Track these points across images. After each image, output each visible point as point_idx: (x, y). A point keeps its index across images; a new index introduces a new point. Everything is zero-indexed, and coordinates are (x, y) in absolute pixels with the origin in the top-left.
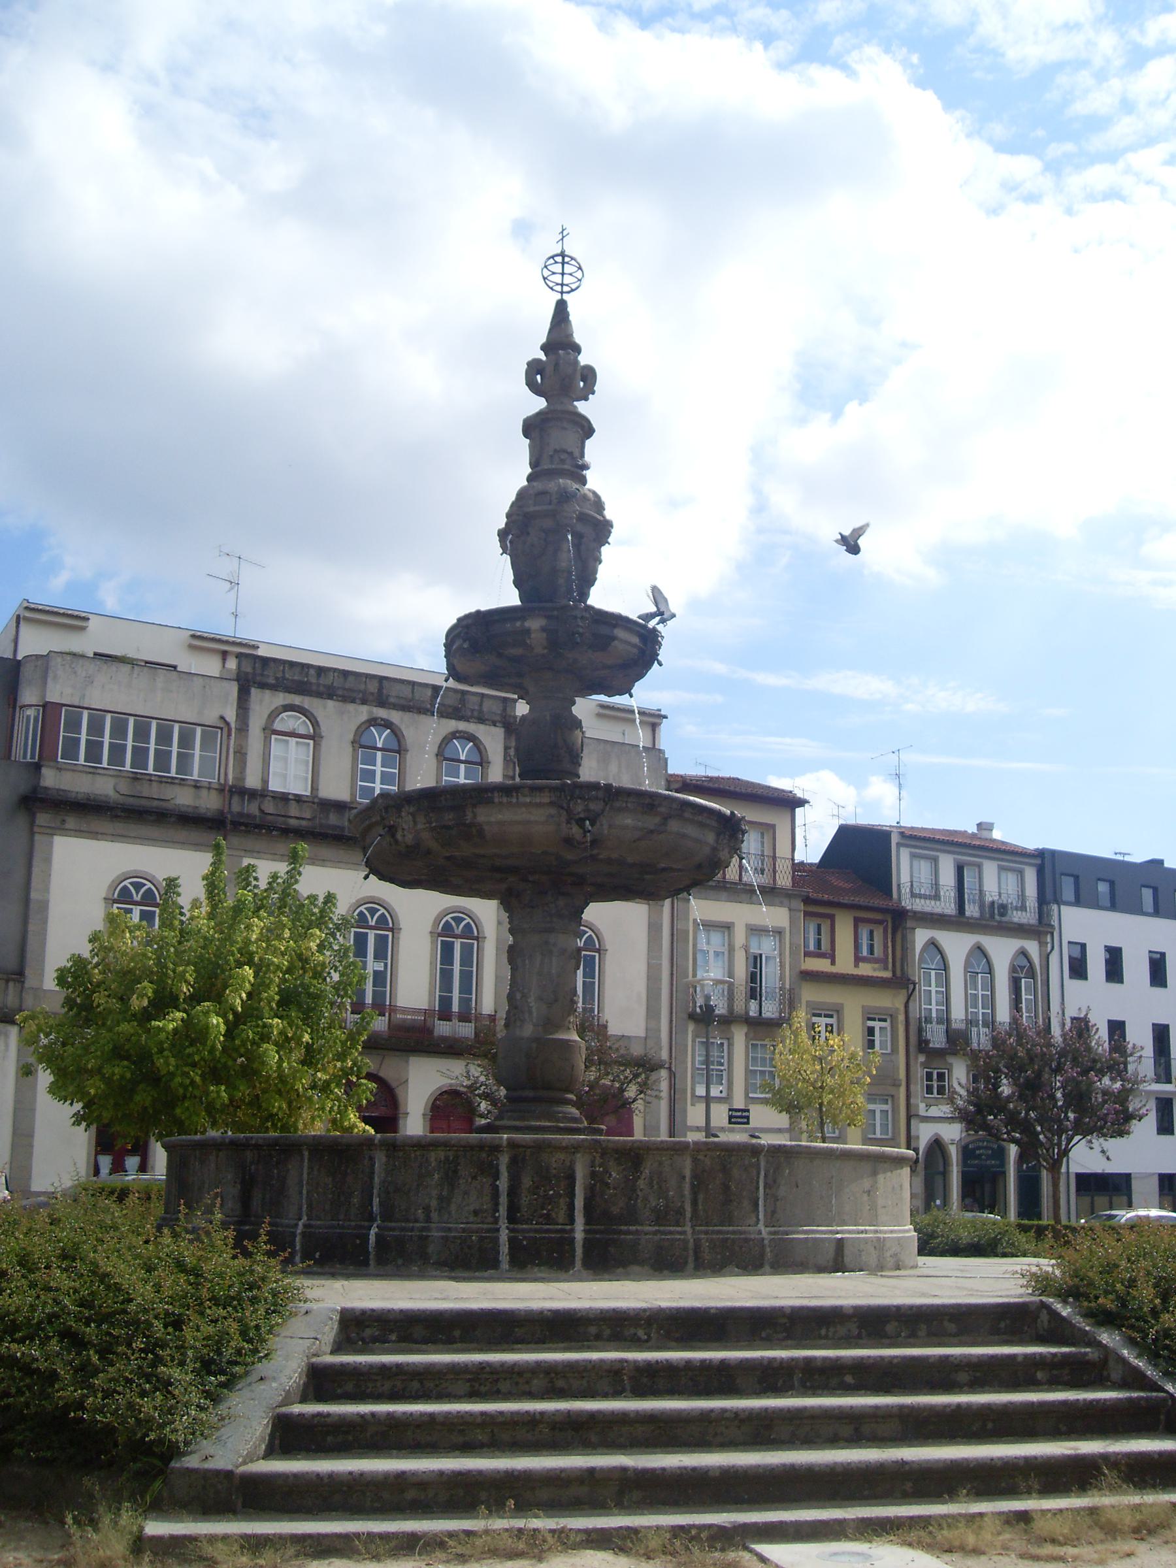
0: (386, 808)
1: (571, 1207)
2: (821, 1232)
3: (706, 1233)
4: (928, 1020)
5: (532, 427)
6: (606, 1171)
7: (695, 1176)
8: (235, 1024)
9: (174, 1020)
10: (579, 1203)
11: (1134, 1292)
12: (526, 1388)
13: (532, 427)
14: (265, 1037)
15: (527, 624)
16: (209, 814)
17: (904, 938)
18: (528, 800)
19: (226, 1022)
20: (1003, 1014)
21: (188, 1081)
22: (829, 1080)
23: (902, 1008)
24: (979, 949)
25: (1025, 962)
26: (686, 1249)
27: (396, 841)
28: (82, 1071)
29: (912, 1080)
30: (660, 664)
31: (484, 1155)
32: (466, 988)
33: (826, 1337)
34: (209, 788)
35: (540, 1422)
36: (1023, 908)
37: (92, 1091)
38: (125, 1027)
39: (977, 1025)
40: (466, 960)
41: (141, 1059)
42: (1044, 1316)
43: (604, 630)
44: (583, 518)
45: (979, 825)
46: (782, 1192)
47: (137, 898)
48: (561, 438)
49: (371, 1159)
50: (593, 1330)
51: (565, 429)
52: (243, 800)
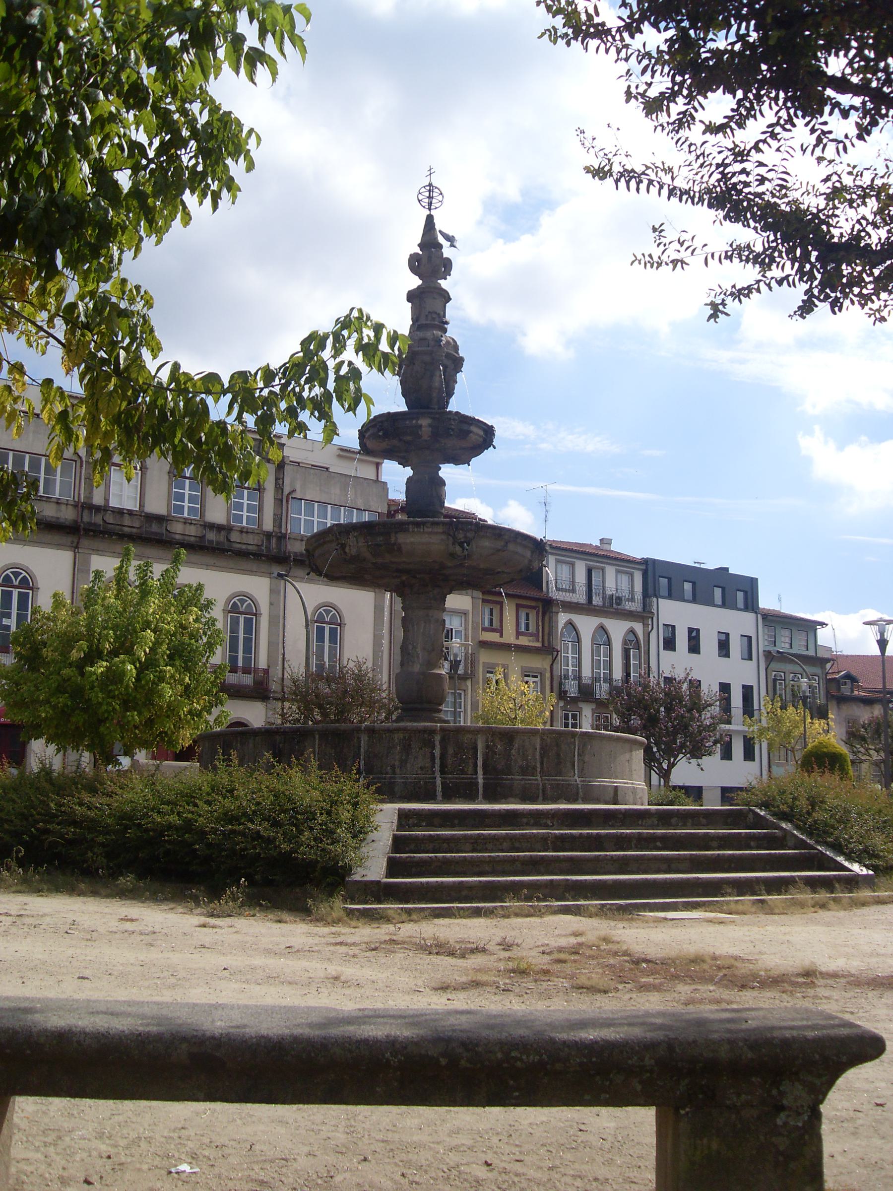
0: (340, 533)
1: (476, 765)
2: (606, 781)
3: (548, 780)
4: (566, 677)
5: (412, 296)
6: (495, 745)
7: (542, 748)
8: (142, 669)
9: (101, 667)
10: (480, 762)
11: (797, 803)
12: (500, 847)
13: (412, 296)
14: (161, 679)
15: (420, 422)
16: (67, 523)
17: (550, 619)
18: (430, 530)
19: (136, 668)
20: (618, 674)
21: (111, 708)
22: (520, 714)
23: (549, 669)
24: (602, 628)
25: (632, 637)
26: (538, 789)
27: (345, 553)
28: (35, 701)
29: (555, 719)
30: (494, 447)
31: (426, 736)
32: (247, 649)
33: (642, 825)
34: (67, 504)
35: (517, 861)
36: (632, 600)
37: (43, 715)
38: (66, 672)
39: (599, 682)
40: (248, 630)
41: (77, 693)
42: (751, 816)
43: (465, 427)
44: (448, 356)
45: (601, 540)
46: (586, 758)
47: (16, 583)
48: (431, 304)
49: (359, 738)
50: (525, 820)
51: (434, 298)
52: (91, 514)
